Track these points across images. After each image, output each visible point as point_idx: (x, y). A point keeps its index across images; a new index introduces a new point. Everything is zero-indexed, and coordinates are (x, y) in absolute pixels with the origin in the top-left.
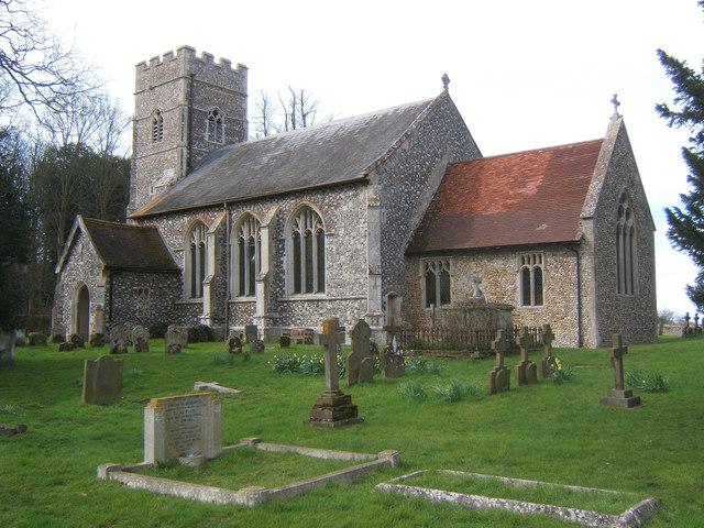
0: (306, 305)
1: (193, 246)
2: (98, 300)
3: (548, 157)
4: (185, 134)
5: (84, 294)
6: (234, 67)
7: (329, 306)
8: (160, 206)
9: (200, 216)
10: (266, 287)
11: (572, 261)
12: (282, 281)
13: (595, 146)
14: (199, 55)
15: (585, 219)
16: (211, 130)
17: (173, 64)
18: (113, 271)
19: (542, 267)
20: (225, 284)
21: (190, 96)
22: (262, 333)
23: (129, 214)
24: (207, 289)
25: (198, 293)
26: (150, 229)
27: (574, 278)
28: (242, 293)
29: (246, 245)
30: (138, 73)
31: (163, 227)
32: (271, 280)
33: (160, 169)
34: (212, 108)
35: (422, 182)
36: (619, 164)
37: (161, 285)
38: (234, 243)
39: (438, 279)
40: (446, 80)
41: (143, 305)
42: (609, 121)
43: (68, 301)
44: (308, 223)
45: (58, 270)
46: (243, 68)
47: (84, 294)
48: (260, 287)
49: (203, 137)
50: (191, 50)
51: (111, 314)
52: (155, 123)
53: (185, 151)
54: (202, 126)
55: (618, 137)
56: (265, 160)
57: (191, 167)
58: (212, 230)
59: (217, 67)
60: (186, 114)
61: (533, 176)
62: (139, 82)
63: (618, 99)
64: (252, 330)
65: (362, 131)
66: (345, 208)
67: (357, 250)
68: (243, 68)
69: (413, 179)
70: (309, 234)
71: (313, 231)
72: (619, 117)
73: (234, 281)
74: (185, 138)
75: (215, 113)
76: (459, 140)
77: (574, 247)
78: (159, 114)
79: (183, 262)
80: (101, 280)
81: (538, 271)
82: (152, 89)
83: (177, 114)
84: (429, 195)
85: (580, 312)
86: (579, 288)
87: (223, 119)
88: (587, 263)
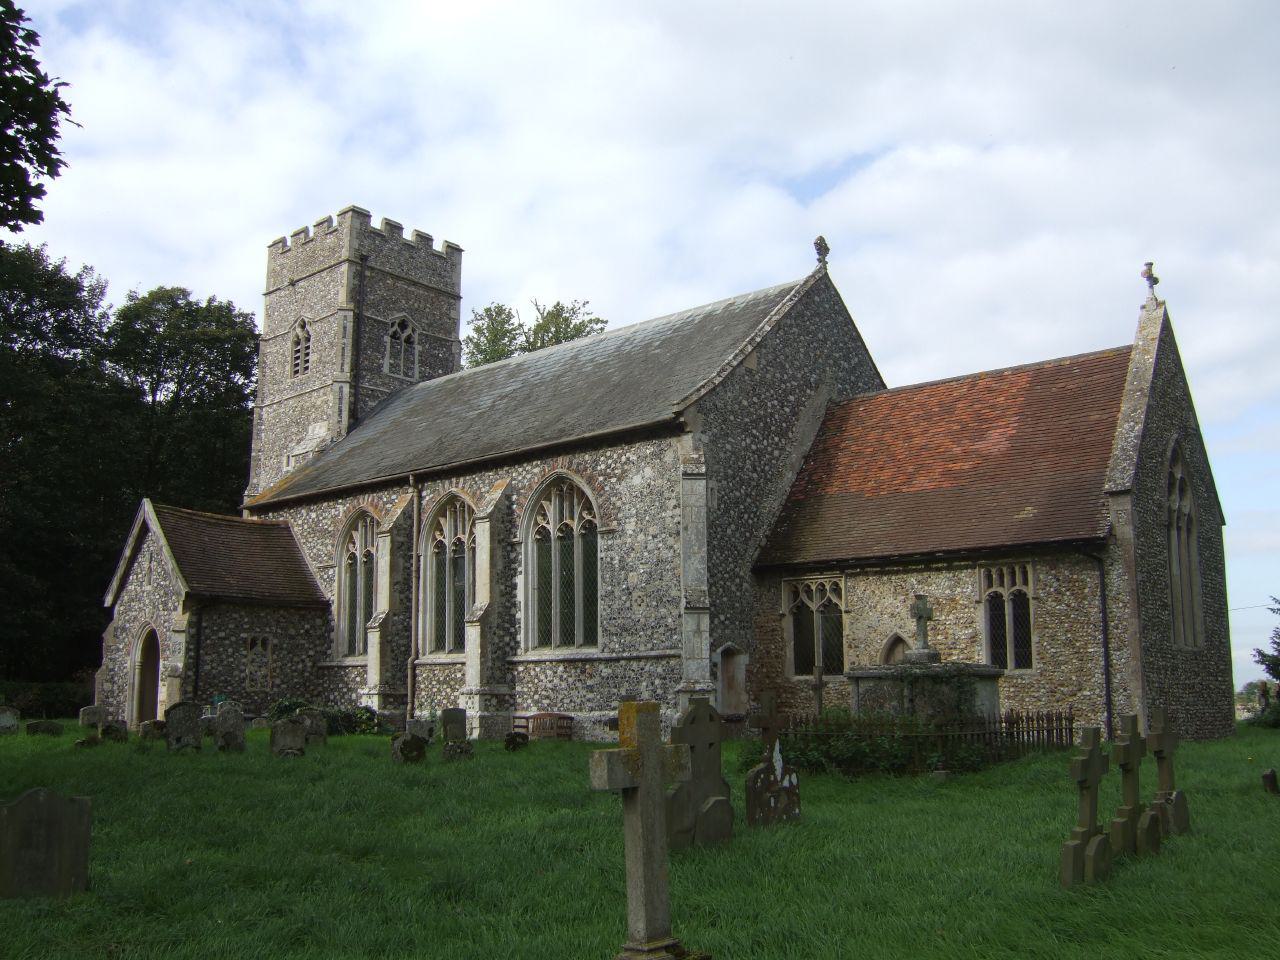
0: (561, 668)
1: (353, 557)
2: (173, 659)
3: (1023, 382)
4: (348, 360)
5: (152, 647)
6: (438, 246)
7: (606, 671)
8: (286, 491)
9: (365, 502)
10: (483, 635)
11: (1090, 578)
12: (513, 621)
13: (1120, 358)
14: (376, 223)
15: (1112, 494)
16: (395, 355)
17: (331, 240)
18: (200, 604)
19: (1030, 591)
20: (408, 629)
21: (358, 295)
22: (476, 723)
23: (247, 501)
24: (374, 638)
25: (360, 646)
26: (276, 526)
27: (1095, 612)
28: (440, 645)
29: (449, 555)
30: (272, 258)
31: (299, 523)
32: (495, 620)
33: (301, 423)
34: (398, 316)
35: (783, 434)
36: (1164, 394)
37: (292, 632)
38: (425, 552)
39: (817, 619)
40: (822, 248)
41: (256, 669)
42: (1138, 312)
43: (124, 658)
44: (566, 513)
45: (108, 600)
46: (454, 251)
47: (152, 647)
48: (473, 634)
49: (380, 366)
50: (361, 215)
51: (196, 682)
52: (298, 343)
53: (346, 389)
54: (378, 346)
55: (1163, 330)
56: (486, 401)
57: (356, 419)
58: (387, 526)
59: (407, 245)
60: (350, 326)
61: (998, 418)
62: (273, 274)
63: (1156, 273)
64: (455, 717)
65: (666, 343)
66: (637, 480)
67: (660, 561)
68: (454, 251)
69: (767, 426)
70: (566, 532)
71: (575, 525)
72: (1159, 304)
73: (424, 625)
74: (347, 368)
75: (403, 325)
76: (847, 358)
77: (1092, 551)
78: (303, 326)
79: (333, 589)
80: (180, 618)
81: (1020, 601)
82: (293, 283)
83: (335, 327)
84: (795, 456)
85: (1108, 681)
86: (1105, 631)
87: (416, 337)
88: (1119, 579)
